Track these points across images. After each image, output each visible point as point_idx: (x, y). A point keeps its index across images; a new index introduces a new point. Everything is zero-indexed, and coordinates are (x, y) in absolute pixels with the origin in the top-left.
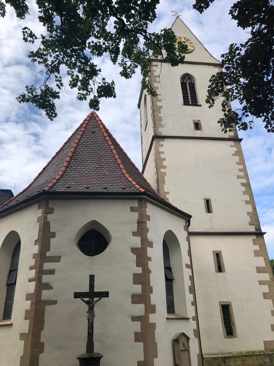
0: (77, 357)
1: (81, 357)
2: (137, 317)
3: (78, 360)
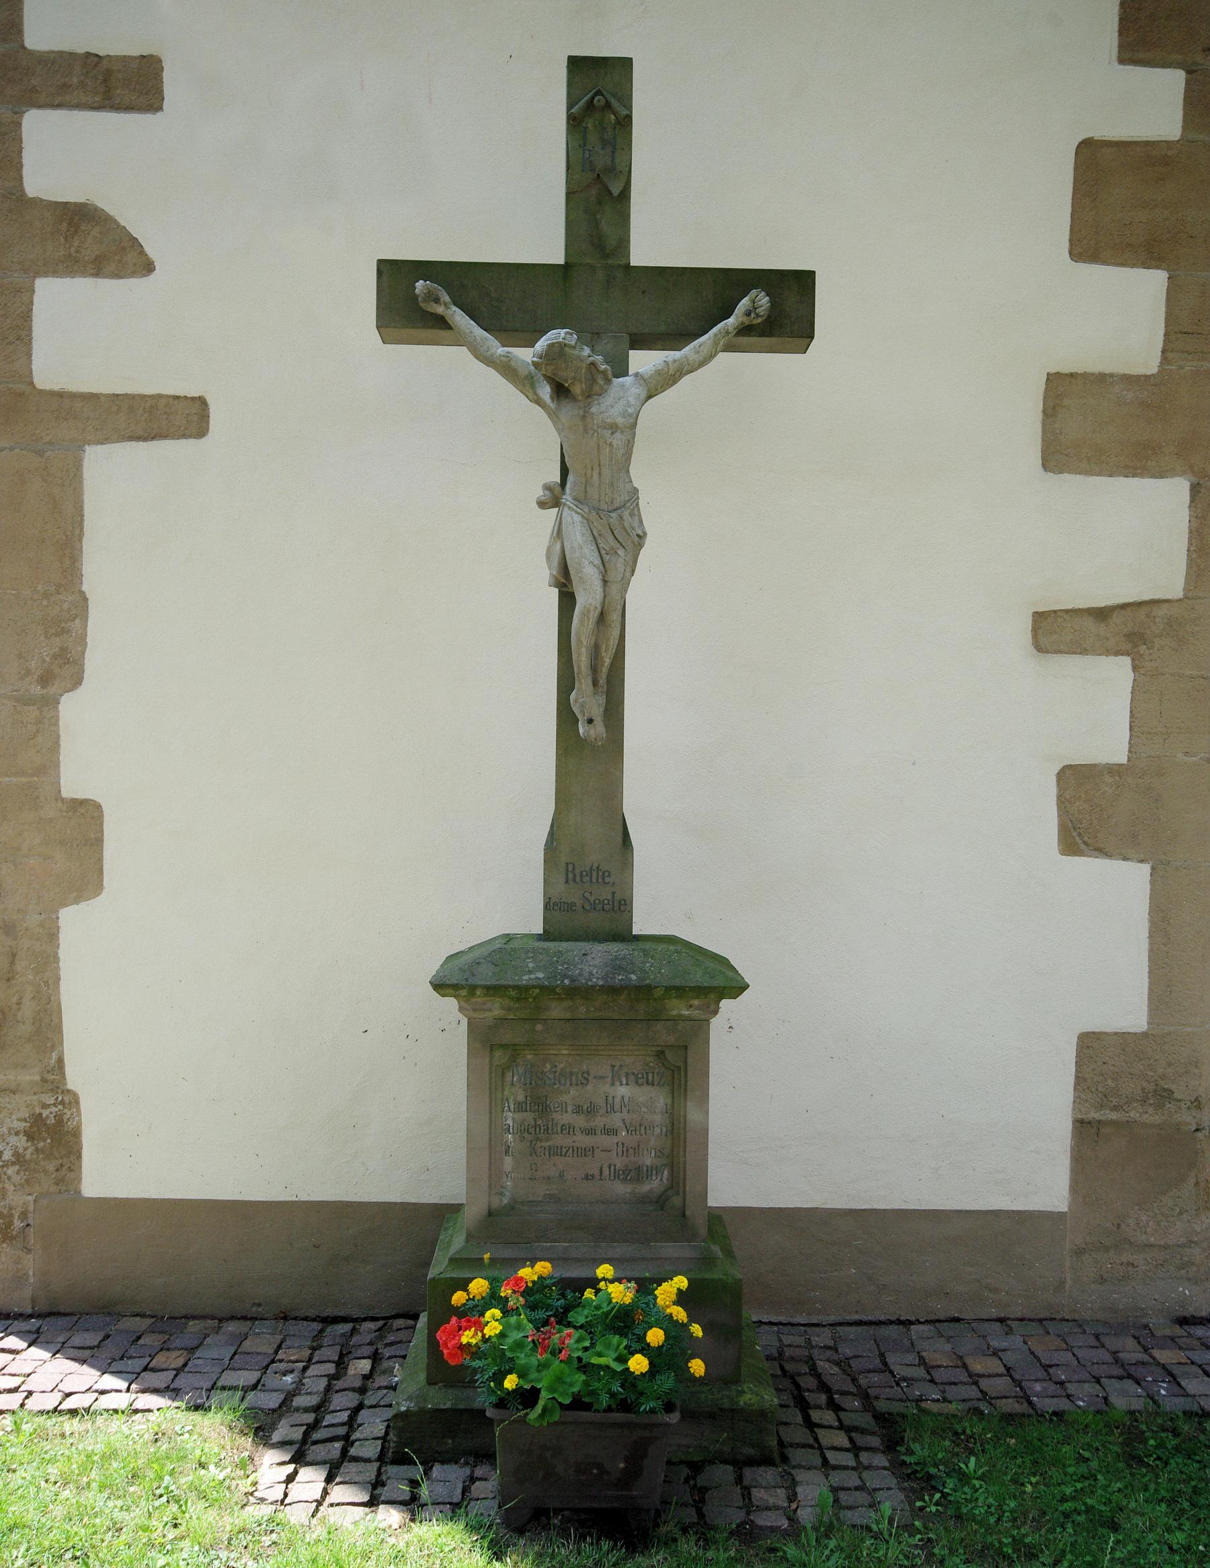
0: (433, 967)
1: (485, 975)
2: (1101, 614)
3: (451, 1003)
